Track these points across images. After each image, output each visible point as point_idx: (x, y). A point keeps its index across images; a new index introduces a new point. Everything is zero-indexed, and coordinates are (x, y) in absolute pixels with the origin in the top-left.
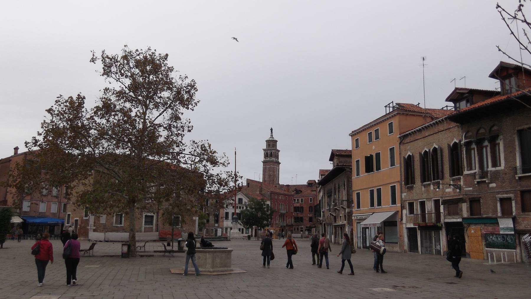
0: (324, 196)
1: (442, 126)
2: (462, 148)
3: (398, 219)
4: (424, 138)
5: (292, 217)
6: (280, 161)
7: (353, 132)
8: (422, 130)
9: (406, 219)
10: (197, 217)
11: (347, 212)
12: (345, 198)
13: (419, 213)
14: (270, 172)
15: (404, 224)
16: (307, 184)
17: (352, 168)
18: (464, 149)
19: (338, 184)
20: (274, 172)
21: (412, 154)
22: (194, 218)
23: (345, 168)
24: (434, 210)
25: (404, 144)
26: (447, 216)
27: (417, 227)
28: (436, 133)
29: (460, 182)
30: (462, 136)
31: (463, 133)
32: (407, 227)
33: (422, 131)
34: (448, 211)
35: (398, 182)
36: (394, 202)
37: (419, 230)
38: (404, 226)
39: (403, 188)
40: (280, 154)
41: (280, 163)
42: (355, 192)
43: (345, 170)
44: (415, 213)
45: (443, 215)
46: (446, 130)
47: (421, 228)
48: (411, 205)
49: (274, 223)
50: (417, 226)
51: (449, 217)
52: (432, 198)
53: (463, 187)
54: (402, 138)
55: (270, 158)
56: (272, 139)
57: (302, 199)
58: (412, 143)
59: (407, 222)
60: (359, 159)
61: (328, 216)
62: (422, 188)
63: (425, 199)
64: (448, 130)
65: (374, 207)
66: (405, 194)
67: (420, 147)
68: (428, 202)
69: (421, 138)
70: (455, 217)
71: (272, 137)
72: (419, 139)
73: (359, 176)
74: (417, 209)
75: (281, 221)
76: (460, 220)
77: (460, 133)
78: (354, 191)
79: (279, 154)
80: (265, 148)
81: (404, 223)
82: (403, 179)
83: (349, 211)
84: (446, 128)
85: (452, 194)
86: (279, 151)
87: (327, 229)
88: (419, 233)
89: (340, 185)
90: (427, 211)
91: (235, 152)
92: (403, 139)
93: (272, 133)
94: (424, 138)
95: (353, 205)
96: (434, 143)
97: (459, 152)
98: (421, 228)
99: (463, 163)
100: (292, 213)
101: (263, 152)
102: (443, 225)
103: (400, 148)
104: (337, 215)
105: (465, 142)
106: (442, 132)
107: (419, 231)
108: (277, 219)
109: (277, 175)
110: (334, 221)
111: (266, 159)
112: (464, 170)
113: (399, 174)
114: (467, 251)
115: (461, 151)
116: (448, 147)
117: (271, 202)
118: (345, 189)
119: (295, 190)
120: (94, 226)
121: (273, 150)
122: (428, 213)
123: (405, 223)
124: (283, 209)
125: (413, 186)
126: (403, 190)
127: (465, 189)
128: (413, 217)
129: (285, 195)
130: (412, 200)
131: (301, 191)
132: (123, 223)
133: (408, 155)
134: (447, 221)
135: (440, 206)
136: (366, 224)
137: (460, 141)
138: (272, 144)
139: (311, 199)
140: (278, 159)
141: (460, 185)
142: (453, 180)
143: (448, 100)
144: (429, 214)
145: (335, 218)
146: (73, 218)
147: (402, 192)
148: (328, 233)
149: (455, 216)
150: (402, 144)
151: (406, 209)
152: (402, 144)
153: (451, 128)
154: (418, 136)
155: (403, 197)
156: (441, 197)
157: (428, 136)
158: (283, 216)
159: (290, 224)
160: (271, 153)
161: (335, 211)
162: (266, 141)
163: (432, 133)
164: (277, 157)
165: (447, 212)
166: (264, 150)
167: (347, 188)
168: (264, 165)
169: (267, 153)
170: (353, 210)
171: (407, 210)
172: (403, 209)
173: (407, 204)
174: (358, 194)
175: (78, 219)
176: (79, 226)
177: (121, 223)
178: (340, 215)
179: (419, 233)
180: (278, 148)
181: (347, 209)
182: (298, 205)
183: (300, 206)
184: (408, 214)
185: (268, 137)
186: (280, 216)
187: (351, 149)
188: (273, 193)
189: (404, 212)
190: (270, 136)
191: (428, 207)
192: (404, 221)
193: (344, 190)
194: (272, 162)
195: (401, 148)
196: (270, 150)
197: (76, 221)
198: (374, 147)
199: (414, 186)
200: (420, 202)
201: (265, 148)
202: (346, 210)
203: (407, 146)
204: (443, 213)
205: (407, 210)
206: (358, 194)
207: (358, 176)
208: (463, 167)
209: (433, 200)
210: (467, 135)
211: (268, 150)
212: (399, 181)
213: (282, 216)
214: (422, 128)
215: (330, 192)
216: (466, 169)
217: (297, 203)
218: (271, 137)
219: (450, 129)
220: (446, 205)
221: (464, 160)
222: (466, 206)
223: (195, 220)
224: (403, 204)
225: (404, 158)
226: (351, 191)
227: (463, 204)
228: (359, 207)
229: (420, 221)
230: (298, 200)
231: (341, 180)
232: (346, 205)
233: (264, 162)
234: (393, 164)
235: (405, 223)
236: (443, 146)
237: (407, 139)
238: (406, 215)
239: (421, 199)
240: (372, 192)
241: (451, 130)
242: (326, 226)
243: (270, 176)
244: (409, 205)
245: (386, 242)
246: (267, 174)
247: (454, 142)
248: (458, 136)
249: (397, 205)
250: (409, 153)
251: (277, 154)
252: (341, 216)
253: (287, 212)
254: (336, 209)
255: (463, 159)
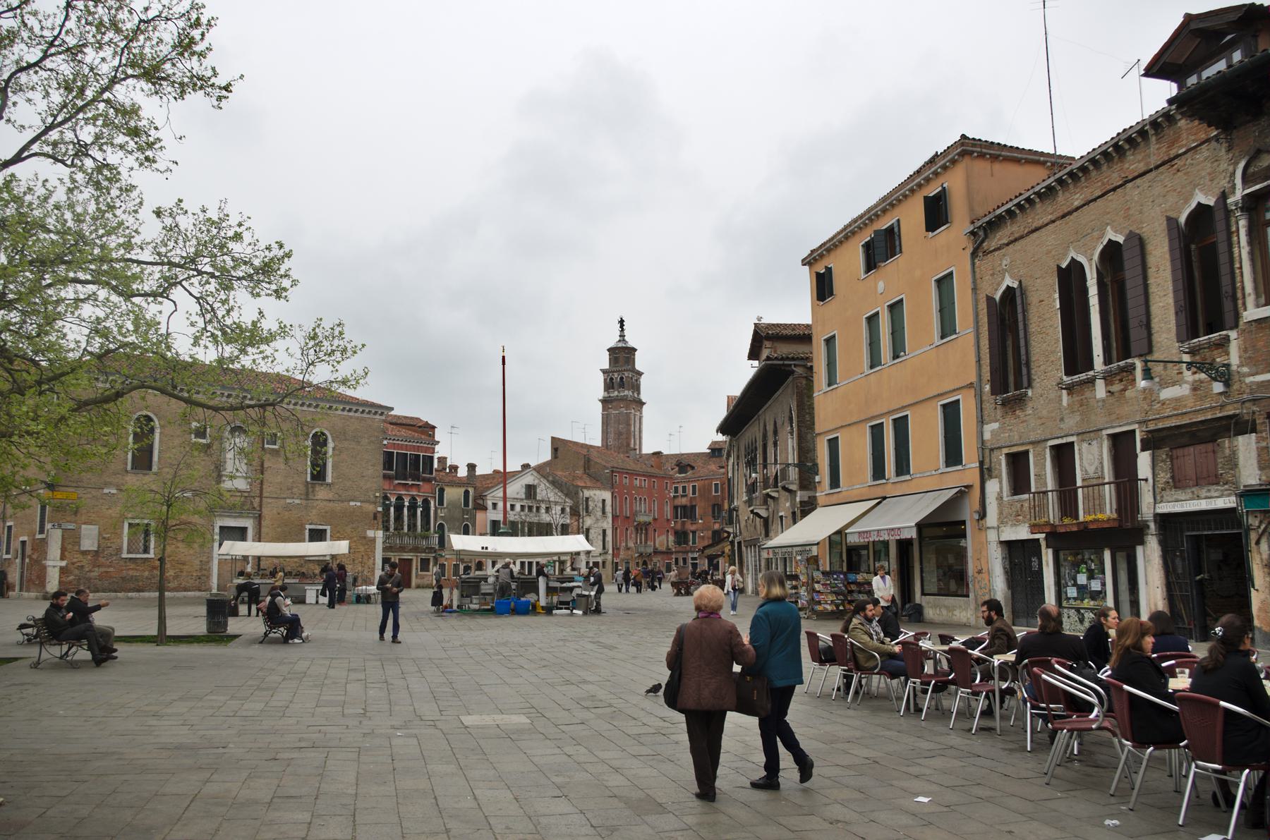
0: (738, 465)
1: (1139, 157)
2: (1233, 220)
3: (968, 513)
4: (1064, 216)
5: (668, 531)
6: (643, 397)
7: (813, 252)
8: (1059, 188)
9: (1001, 513)
10: (377, 529)
11: (801, 502)
12: (792, 457)
13: (1049, 488)
14: (619, 424)
15: (992, 530)
16: (708, 451)
17: (812, 367)
18: (1243, 223)
19: (772, 423)
20: (629, 425)
21: (1020, 282)
22: (370, 533)
23: (791, 365)
24: (1111, 472)
25: (986, 253)
26: (1168, 492)
27: (1041, 536)
28: (1114, 189)
29: (1228, 354)
30: (1234, 173)
31: (1236, 164)
32: (1001, 539)
33: (1057, 192)
34: (1172, 470)
35: (971, 385)
36: (953, 455)
37: (1048, 547)
38: (992, 536)
39: (988, 406)
40: (643, 380)
41: (644, 403)
42: (822, 436)
43: (793, 372)
44: (1033, 490)
45: (1151, 488)
46: (1157, 167)
47: (1057, 539)
48: (1018, 463)
49: (622, 548)
50: (1044, 535)
51: (1180, 494)
52: (1101, 430)
53: (1239, 372)
54: (981, 233)
55: (619, 392)
56: (624, 345)
57: (694, 487)
58: (1017, 243)
59: (1002, 521)
60: (835, 332)
61: (748, 518)
62: (1060, 397)
63: (1072, 435)
64: (1166, 166)
65: (884, 481)
66: (995, 426)
67: (1049, 252)
68: (1085, 445)
69: (1053, 221)
70: (1203, 493)
71: (624, 340)
72: (1047, 225)
73: (836, 386)
74: (1043, 473)
75: (641, 543)
76: (1225, 502)
77: (1224, 166)
78: (819, 434)
79: (641, 380)
80: (606, 366)
81: (993, 528)
82: (987, 375)
83: (806, 499)
84: (1154, 160)
85: (1190, 405)
86: (640, 374)
87: (747, 557)
88: (1048, 556)
89: (779, 423)
90: (1083, 480)
91: (504, 357)
92: (986, 236)
93: (622, 330)
94: (1064, 216)
95: (817, 480)
96: (1109, 228)
97: (1221, 237)
98: (1057, 539)
99: (1238, 279)
100: (668, 520)
101: (601, 377)
102: (1152, 525)
103: (974, 272)
104: (771, 516)
105: (1244, 197)
106: (1138, 181)
107: (1050, 551)
108: (631, 538)
109: (637, 433)
110: (763, 532)
111: (608, 393)
112: (1244, 304)
113: (973, 359)
114: (1256, 623)
115: (1229, 234)
116: (1170, 230)
117: (612, 493)
118: (792, 433)
119: (677, 465)
120: (62, 559)
121: (627, 371)
122: (1086, 484)
123: (995, 524)
124: (645, 512)
125: (1026, 394)
126: (986, 413)
127: (1249, 380)
128: (1026, 505)
129: (650, 476)
130: (1022, 444)
131: (693, 468)
132: (152, 551)
133: (1004, 287)
134: (1164, 508)
135: (1136, 456)
136: (867, 532)
137: (1224, 196)
138: (622, 356)
139: (716, 485)
140: (639, 394)
141: (1228, 366)
142: (1192, 352)
143: (1155, 69)
144: (1088, 487)
145: (766, 523)
146: (17, 537)
147: (982, 421)
148: (748, 570)
149: (1204, 491)
150: (981, 254)
151: (999, 477)
152: (981, 254)
153: (1177, 156)
154: (1042, 213)
155: (987, 436)
156: (1139, 423)
157: (1084, 205)
158: (646, 530)
159: (664, 549)
160: (622, 378)
161: (765, 503)
162: (609, 350)
163: (1098, 193)
164: (637, 388)
165: (1169, 475)
166: (604, 372)
167: (798, 426)
168: (604, 409)
169: (611, 379)
170: (817, 495)
171: (1001, 482)
172: (986, 476)
173: (1003, 458)
174: (833, 444)
175: (25, 538)
176: (27, 560)
177: (146, 550)
178: (780, 514)
179: (1048, 556)
180: (638, 366)
181: (799, 493)
182: (684, 501)
183: (689, 504)
184: (1005, 494)
185: (613, 341)
186: (637, 530)
187: (810, 322)
188: (616, 472)
189: (992, 487)
190: (618, 338)
191: (1085, 463)
192: (992, 518)
193: (789, 436)
194: (624, 399)
195: (977, 270)
196: (619, 371)
197: (23, 543)
198: (881, 285)
199: (1030, 393)
200: (1052, 447)
201: (606, 366)
202: (796, 496)
203: (1001, 260)
204: (1151, 481)
205: (1001, 482)
206: (833, 444)
207: (831, 388)
208: (1239, 295)
209: (1105, 437)
210: (1251, 170)
211: (614, 372)
212: (971, 383)
213: (641, 530)
214: (1056, 181)
215: (752, 450)
216: (1250, 301)
217: (682, 496)
218: (620, 341)
219: (1176, 161)
220: (1163, 454)
221: (1241, 268)
222: (1254, 446)
223: (374, 540)
224: (987, 460)
225: (990, 300)
226: (809, 436)
227: (1240, 438)
228: (835, 482)
229: (1052, 513)
230: (684, 488)
231: (783, 404)
232: (797, 482)
233: (605, 401)
234: (947, 328)
235: (995, 524)
236: (1144, 230)
237: (999, 235)
238: (1000, 498)
239: (1058, 438)
240: (877, 431)
241: (1178, 162)
242: (744, 548)
243: (619, 434)
244: (1008, 464)
245: (925, 592)
246: (611, 430)
247: (1193, 205)
248: (1212, 180)
249: (968, 466)
250: (1009, 282)
251: (637, 380)
252: (781, 517)
253: (655, 519)
254: (768, 495)
255: (1237, 265)
